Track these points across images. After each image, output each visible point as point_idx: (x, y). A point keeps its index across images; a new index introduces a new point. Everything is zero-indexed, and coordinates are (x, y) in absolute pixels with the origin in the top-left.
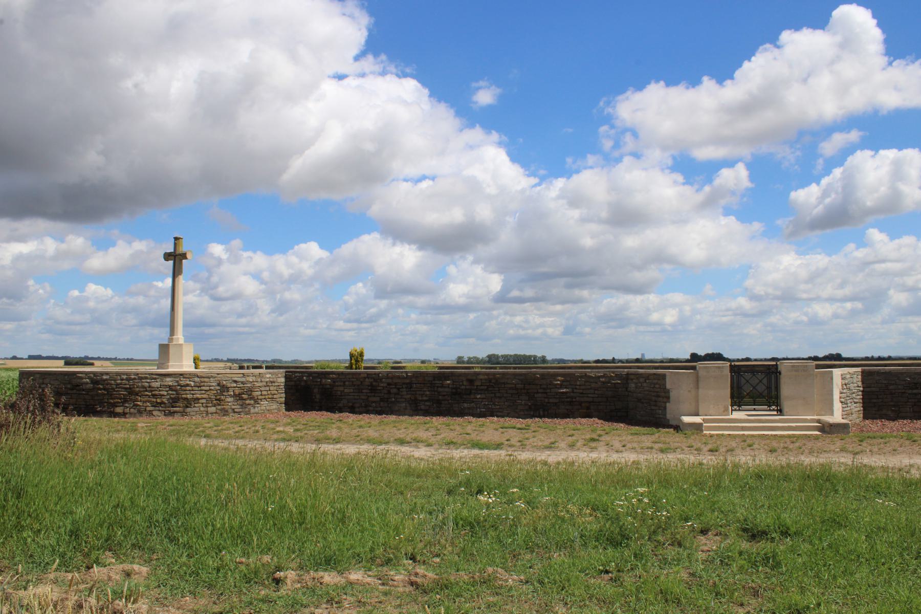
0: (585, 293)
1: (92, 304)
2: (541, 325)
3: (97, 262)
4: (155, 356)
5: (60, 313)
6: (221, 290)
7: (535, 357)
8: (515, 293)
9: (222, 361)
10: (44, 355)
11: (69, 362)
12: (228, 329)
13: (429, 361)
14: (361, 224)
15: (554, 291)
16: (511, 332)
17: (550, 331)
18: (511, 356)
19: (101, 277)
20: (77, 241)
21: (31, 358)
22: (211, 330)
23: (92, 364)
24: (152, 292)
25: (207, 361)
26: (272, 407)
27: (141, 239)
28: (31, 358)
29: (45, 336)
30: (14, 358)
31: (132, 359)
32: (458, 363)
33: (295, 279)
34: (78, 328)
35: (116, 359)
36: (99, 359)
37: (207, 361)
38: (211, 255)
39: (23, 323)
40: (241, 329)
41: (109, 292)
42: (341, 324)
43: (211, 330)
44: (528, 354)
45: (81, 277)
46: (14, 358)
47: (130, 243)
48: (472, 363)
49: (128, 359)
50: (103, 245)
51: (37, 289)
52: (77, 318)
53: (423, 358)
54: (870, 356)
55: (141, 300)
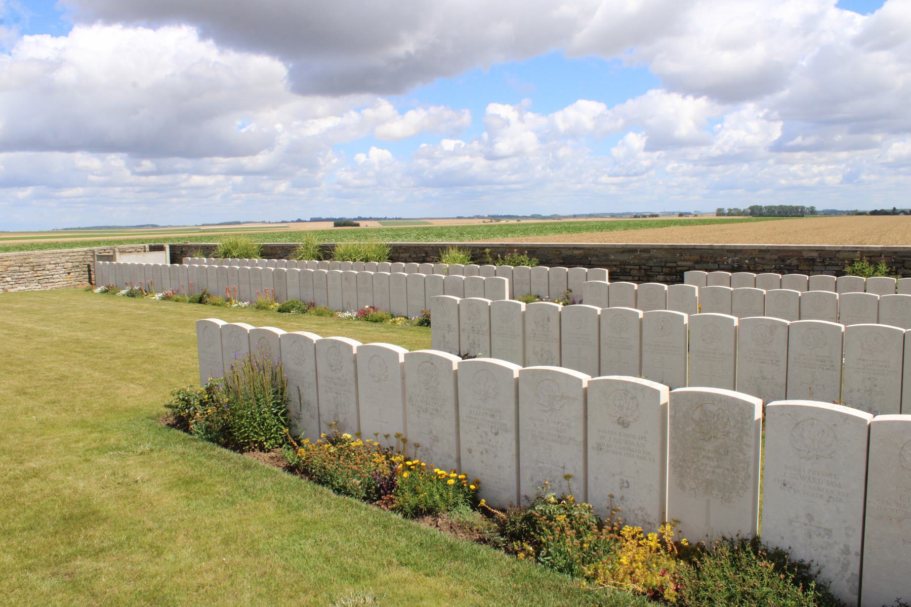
0: (878, 138)
2: (820, 174)
7: (803, 208)
8: (799, 140)
9: (483, 217)
10: (324, 217)
11: (339, 223)
12: (499, 187)
13: (689, 214)
14: (642, 79)
15: (838, 138)
16: (783, 182)
17: (829, 179)
18: (775, 207)
20: (384, 107)
22: (480, 188)
23: (358, 225)
25: (469, 218)
26: (340, 250)
28: (203, 225)
30: (299, 221)
31: (399, 219)
32: (718, 215)
33: (573, 134)
35: (385, 219)
36: (360, 219)
37: (469, 218)
40: (515, 186)
42: (604, 179)
43: (480, 188)
44: (794, 205)
46: (299, 221)
48: (733, 215)
49: (396, 219)
50: (402, 111)
53: (683, 211)
54: (879, 209)
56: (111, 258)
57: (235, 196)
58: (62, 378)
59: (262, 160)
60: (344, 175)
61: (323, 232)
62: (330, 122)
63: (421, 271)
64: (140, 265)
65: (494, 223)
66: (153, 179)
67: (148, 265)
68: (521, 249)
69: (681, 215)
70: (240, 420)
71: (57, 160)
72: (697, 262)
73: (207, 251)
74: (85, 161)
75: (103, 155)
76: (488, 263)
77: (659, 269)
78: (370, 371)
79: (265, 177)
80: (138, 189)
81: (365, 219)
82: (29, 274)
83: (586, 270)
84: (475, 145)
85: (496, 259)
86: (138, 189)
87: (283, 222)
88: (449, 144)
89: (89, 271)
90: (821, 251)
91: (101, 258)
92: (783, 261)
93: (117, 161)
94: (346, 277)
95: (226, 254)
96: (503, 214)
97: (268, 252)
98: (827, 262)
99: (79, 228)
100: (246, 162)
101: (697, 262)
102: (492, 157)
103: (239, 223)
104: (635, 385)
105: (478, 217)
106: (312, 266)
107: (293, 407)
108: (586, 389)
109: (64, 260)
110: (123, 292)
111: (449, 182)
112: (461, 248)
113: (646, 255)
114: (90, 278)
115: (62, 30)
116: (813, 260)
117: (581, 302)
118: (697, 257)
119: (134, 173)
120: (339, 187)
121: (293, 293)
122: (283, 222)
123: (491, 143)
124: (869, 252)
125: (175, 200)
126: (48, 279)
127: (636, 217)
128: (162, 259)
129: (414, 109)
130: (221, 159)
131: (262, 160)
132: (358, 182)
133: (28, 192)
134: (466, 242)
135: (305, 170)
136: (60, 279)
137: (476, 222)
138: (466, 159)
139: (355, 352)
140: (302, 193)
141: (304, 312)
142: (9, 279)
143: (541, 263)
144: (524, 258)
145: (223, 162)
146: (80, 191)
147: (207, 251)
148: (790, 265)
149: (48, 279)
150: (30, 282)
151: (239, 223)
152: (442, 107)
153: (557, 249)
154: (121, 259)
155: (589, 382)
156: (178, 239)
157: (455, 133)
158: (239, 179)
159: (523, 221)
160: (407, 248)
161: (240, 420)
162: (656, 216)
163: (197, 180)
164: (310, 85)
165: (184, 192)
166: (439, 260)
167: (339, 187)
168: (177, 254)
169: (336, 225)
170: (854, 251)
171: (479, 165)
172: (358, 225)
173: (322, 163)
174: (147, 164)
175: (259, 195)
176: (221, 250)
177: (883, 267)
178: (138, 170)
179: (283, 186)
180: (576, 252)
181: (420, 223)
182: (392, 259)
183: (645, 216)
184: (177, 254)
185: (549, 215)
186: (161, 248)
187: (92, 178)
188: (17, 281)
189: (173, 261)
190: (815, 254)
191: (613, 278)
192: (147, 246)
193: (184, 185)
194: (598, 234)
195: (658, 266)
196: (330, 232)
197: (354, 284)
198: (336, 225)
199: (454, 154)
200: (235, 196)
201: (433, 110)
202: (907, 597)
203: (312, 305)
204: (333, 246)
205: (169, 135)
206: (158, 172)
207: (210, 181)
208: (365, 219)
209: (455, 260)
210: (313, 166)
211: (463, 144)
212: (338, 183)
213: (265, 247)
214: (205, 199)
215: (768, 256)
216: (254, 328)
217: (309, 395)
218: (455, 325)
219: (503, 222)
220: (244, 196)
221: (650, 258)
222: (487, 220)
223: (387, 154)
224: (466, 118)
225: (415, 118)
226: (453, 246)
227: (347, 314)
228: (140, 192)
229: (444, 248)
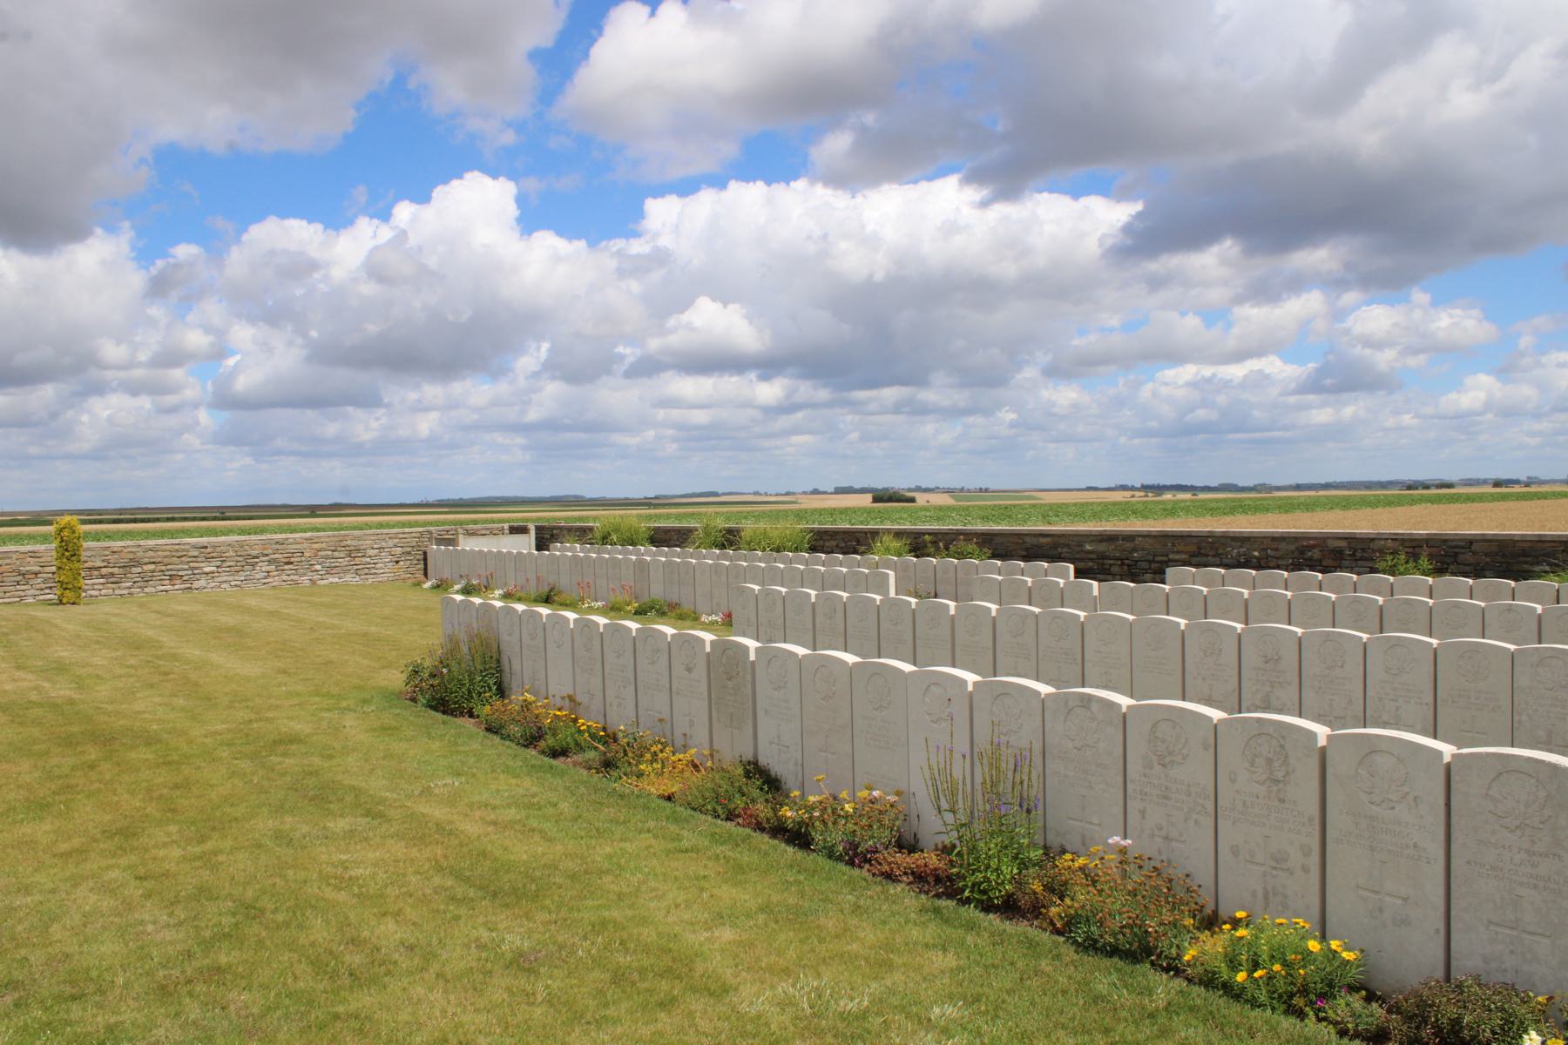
9: (1133, 488)
10: (857, 486)
11: (881, 497)
13: (1517, 482)
23: (912, 500)
30: (816, 492)
31: (986, 490)
35: (962, 490)
36: (919, 489)
56: (452, 542)
58: (329, 663)
61: (854, 510)
63: (841, 565)
64: (481, 552)
65: (1151, 497)
67: (509, 553)
68: (969, 536)
69: (1497, 484)
70: (460, 688)
73: (582, 534)
76: (929, 555)
77: (1144, 565)
78: (567, 650)
81: (927, 490)
82: (344, 562)
83: (1471, 581)
85: (938, 549)
87: (787, 494)
89: (425, 560)
90: (1350, 539)
91: (440, 542)
92: (1302, 553)
94: (716, 569)
95: (605, 539)
96: (1279, 484)
97: (660, 538)
98: (1359, 554)
101: (1193, 555)
104: (1182, 709)
105: (1124, 488)
106: (710, 558)
107: (506, 678)
108: (1323, 749)
109: (391, 543)
110: (457, 587)
112: (898, 534)
113: (1129, 545)
114: (426, 569)
117: (936, 596)
118: (1193, 548)
121: (657, 591)
122: (787, 494)
124: (1412, 540)
126: (369, 570)
127: (1410, 488)
128: (525, 544)
134: (908, 526)
136: (385, 569)
137: (1119, 496)
139: (970, 688)
141: (664, 614)
142: (318, 567)
143: (994, 556)
144: (971, 547)
147: (582, 534)
148: (1311, 559)
149: (369, 570)
150: (345, 572)
151: (716, 494)
153: (1322, 541)
155: (1329, 737)
156: (518, 520)
159: (1202, 496)
160: (833, 534)
161: (460, 688)
162: (1450, 486)
166: (869, 550)
168: (545, 538)
169: (876, 500)
170: (1395, 538)
172: (912, 500)
176: (598, 535)
180: (1043, 540)
181: (1009, 498)
182: (813, 549)
183: (1427, 487)
184: (545, 538)
185: (1251, 484)
186: (522, 530)
188: (329, 571)
189: (539, 547)
190: (1343, 544)
191: (1079, 573)
192: (506, 526)
194: (1337, 514)
196: (869, 511)
197: (724, 578)
198: (876, 500)
202: (1535, 934)
203: (673, 606)
204: (738, 531)
208: (927, 490)
209: (888, 550)
213: (657, 529)
215: (1283, 546)
216: (859, 659)
217: (516, 666)
218: (754, 620)
219: (1168, 496)
222: (1138, 494)
226: (889, 531)
227: (714, 618)
229: (875, 534)
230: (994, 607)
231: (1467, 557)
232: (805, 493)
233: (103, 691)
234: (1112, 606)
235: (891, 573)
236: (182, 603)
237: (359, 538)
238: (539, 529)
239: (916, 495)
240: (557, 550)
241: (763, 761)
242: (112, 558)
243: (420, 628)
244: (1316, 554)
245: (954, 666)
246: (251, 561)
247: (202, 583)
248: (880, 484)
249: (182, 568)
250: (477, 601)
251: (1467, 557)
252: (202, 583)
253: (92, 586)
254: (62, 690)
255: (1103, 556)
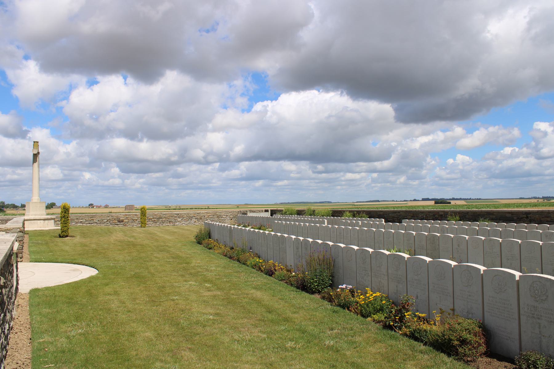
1: (460, 167)
3: (467, 142)
4: (26, 222)
5: (443, 174)
6: (545, 151)
9: (539, 198)
10: (430, 198)
11: (437, 201)
12: (547, 178)
19: (466, 151)
20: (458, 130)
21: (424, 200)
23: (450, 203)
24: (499, 157)
27: (494, 126)
28: (424, 200)
29: (434, 187)
30: (415, 200)
31: (480, 199)
34: (453, 182)
35: (470, 199)
36: (453, 199)
38: (539, 130)
39: (423, 180)
41: (468, 158)
43: (534, 179)
45: (454, 151)
46: (415, 200)
47: (486, 129)
49: (477, 199)
50: (470, 131)
51: (430, 161)
52: (453, 176)
55: (491, 163)
57: (373, 185)
59: (386, 164)
60: (438, 171)
61: (430, 206)
62: (425, 139)
66: (324, 175)
71: (272, 165)
72: (412, 217)
73: (280, 211)
74: (289, 166)
75: (297, 162)
79: (390, 174)
80: (317, 181)
82: (216, 219)
84: (525, 149)
86: (317, 181)
88: (508, 150)
93: (304, 166)
99: (289, 203)
100: (378, 165)
101: (412, 217)
102: (540, 158)
103: (378, 201)
105: (535, 198)
111: (509, 175)
112: (350, 212)
115: (275, 98)
116: (442, 215)
118: (412, 215)
119: (314, 172)
120: (437, 179)
123: (537, 149)
125: (339, 187)
128: (268, 215)
129: (478, 130)
130: (362, 164)
131: (386, 164)
132: (449, 176)
133: (260, 183)
135: (414, 169)
138: (521, 159)
139: (482, 272)
140: (414, 183)
145: (363, 165)
146: (286, 182)
151: (378, 201)
152: (497, 127)
154: (250, 214)
155: (520, 276)
157: (511, 142)
158: (375, 175)
163: (349, 176)
164: (407, 117)
165: (343, 183)
167: (437, 179)
169: (436, 203)
171: (530, 163)
173: (425, 164)
174: (320, 167)
175: (388, 184)
177: (458, 218)
178: (315, 170)
179: (402, 179)
187: (292, 175)
190: (443, 213)
193: (343, 178)
195: (394, 216)
199: (510, 156)
200: (373, 185)
201: (491, 129)
205: (330, 150)
206: (326, 172)
207: (357, 176)
210: (419, 166)
211: (517, 149)
212: (436, 177)
213: (298, 211)
214: (357, 186)
220: (379, 185)
221: (400, 215)
222: (540, 200)
223: (467, 158)
224: (516, 132)
225: (479, 136)
228: (319, 183)
229: (344, 211)
230: (383, 230)
231: (467, 216)
232: (411, 201)
233: (139, 240)
234: (392, 229)
235: (326, 220)
236: (170, 227)
237: (220, 213)
238: (271, 211)
239: (451, 201)
240: (275, 216)
241: (487, 322)
242: (155, 216)
243: (194, 228)
244: (437, 216)
245: (501, 267)
246: (191, 218)
247: (178, 224)
248: (439, 197)
249: (172, 219)
250: (261, 231)
251: (467, 216)
252: (178, 224)
253: (150, 223)
254: (132, 239)
255: (393, 217)
